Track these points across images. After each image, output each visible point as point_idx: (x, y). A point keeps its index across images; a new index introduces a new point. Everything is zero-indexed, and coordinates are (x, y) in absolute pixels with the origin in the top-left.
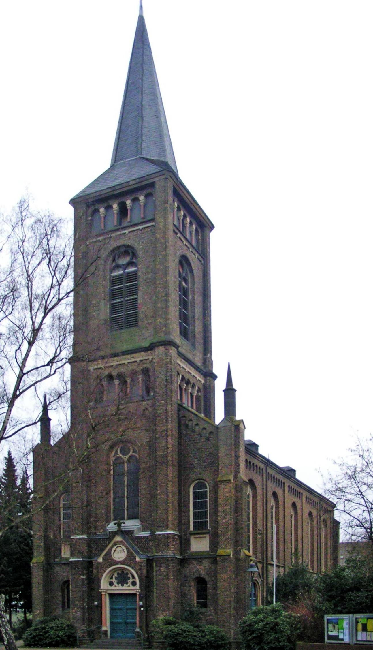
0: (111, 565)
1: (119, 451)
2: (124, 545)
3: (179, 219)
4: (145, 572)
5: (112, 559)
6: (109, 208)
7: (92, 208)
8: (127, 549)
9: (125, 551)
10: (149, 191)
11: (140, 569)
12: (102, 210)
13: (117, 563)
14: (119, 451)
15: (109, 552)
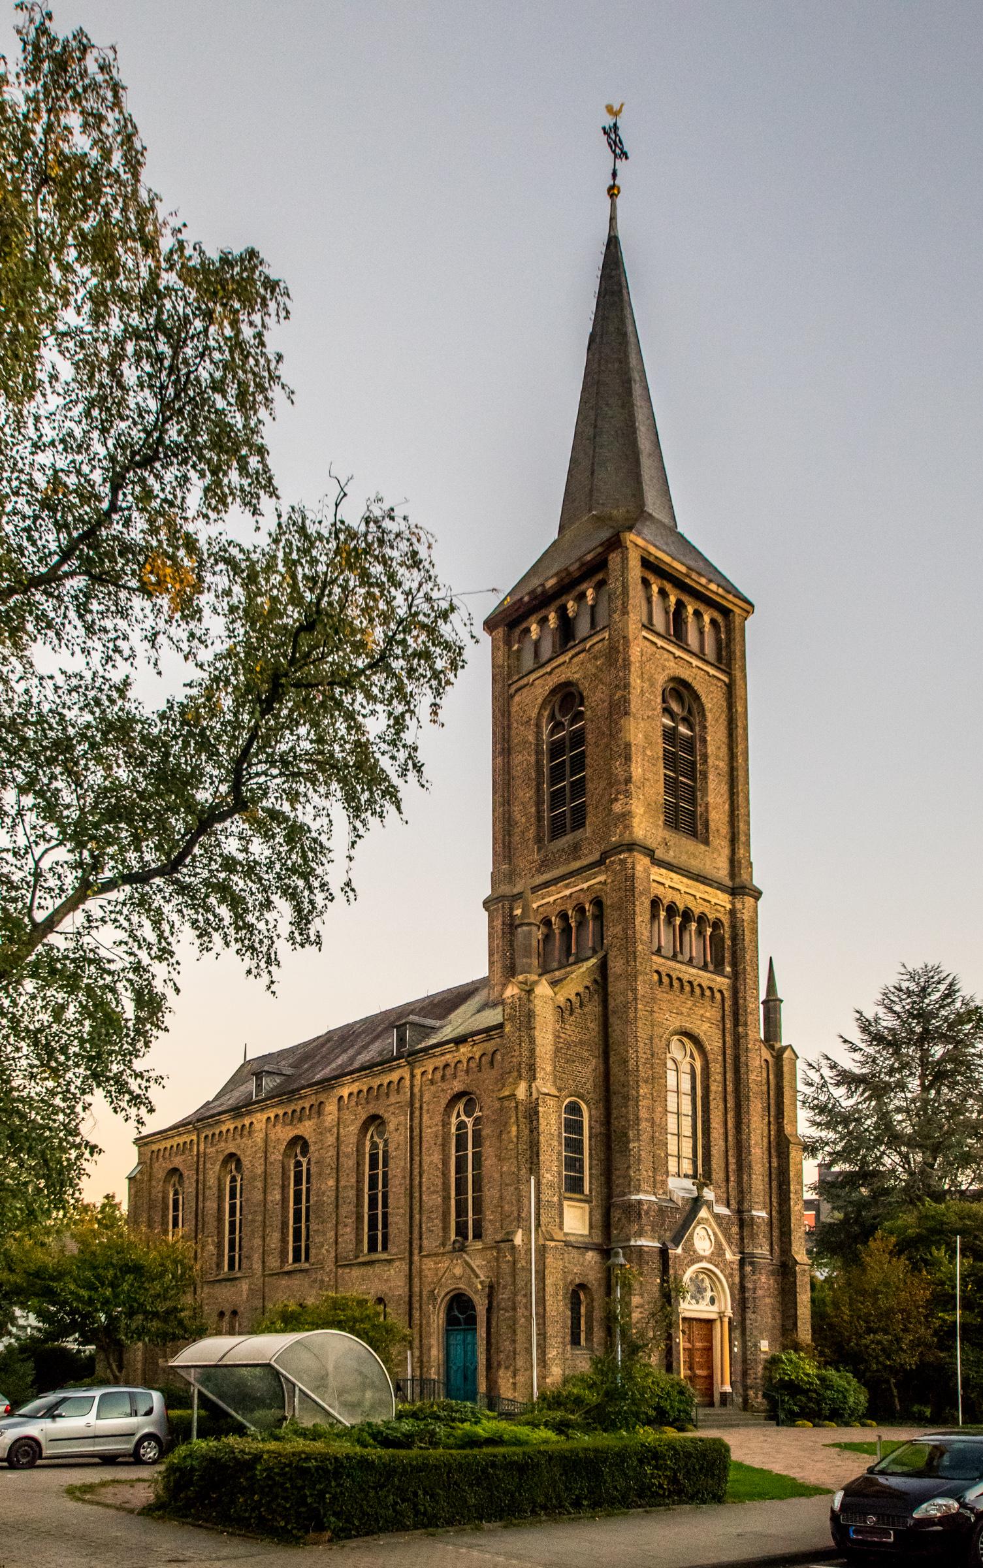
0: (693, 1262)
1: (462, 1113)
2: (710, 1225)
3: (667, 612)
4: (737, 1280)
5: (695, 1251)
6: (543, 621)
7: (517, 631)
8: (715, 1234)
9: (712, 1238)
10: (600, 576)
11: (732, 1274)
12: (534, 628)
13: (701, 1259)
14: (462, 1113)
15: (692, 1235)
